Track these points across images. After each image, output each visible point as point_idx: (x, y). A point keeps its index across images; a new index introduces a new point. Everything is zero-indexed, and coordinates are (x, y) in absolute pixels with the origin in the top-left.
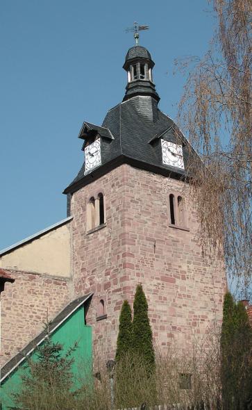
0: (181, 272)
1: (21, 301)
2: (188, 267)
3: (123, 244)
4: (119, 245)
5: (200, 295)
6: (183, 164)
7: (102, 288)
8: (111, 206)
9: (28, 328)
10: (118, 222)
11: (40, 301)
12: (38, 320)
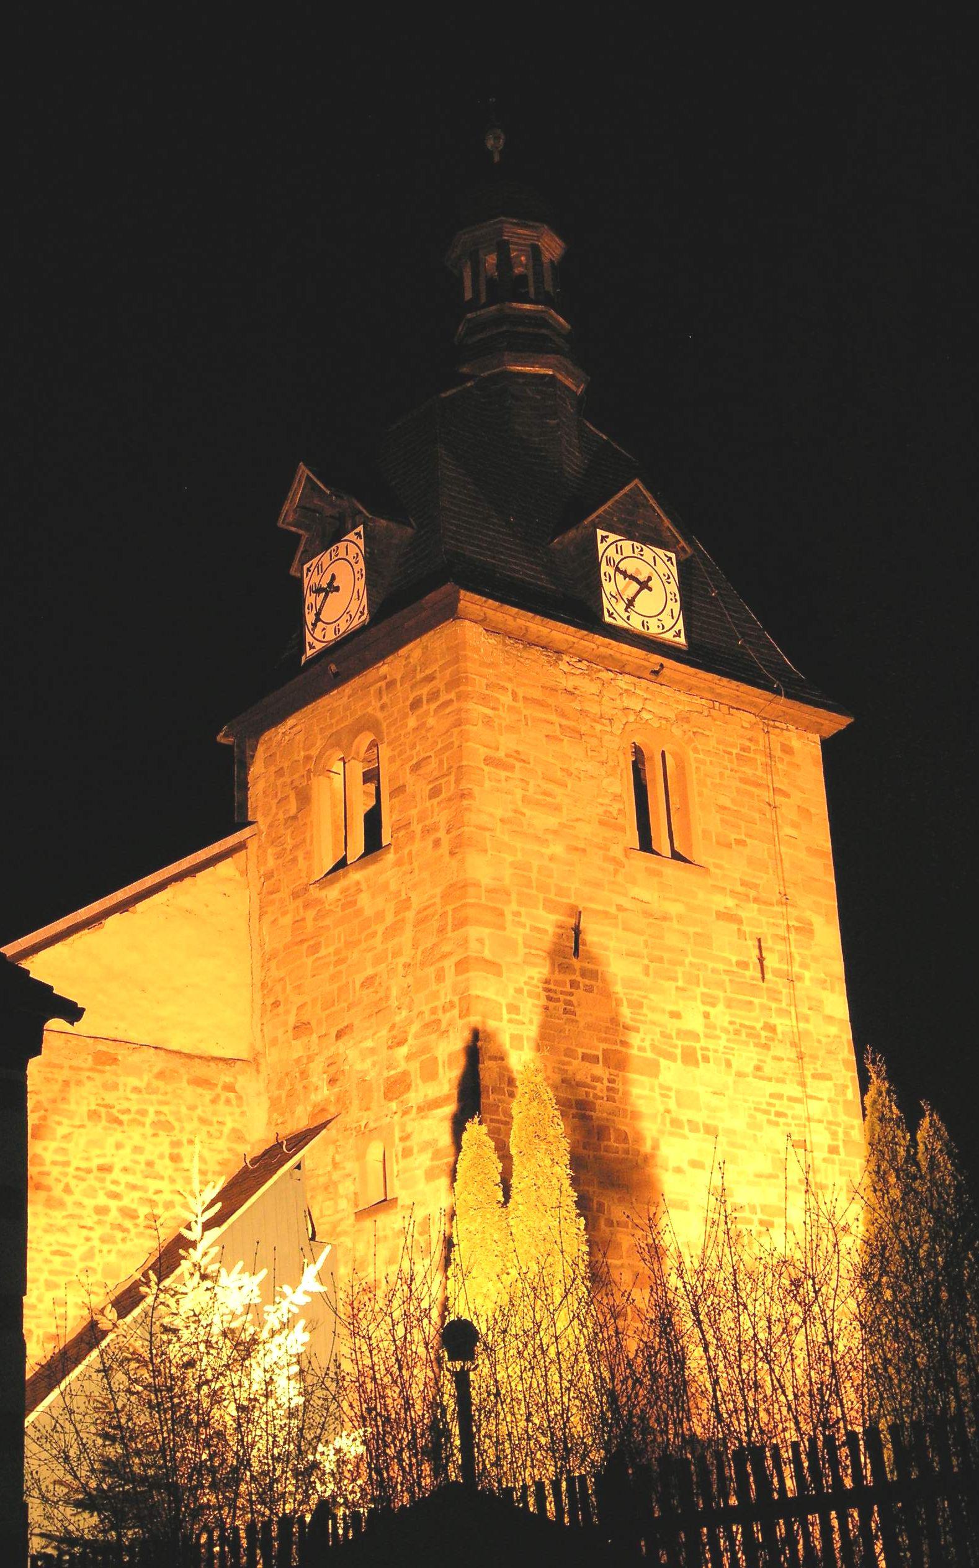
0: (681, 1034)
1: (63, 1151)
2: (706, 1015)
3: (461, 923)
4: (442, 930)
5: (753, 1125)
6: (680, 625)
7: (378, 1095)
8: (409, 779)
9: (89, 1255)
10: (437, 843)
11: (137, 1149)
12: (128, 1224)
